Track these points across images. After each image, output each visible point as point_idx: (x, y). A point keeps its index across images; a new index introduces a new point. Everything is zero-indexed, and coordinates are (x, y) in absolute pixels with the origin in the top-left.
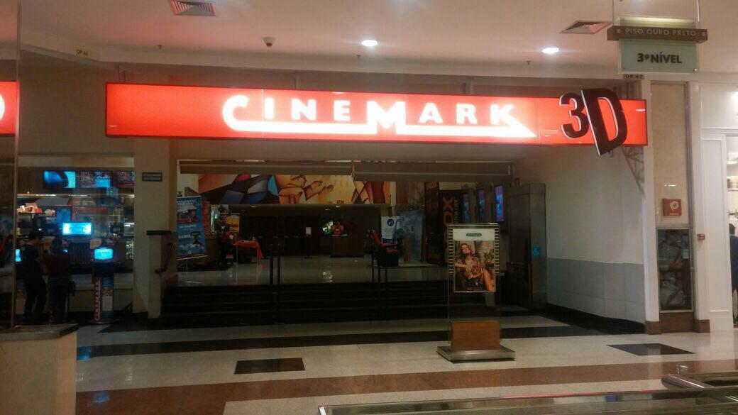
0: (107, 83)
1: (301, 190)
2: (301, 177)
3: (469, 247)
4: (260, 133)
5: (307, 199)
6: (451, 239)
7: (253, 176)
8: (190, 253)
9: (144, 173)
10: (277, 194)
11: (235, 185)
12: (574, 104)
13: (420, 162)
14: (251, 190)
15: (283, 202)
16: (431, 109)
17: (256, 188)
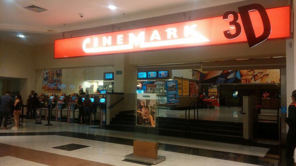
0: (55, 40)
1: (252, 77)
2: (252, 70)
3: (144, 103)
4: (93, 53)
5: (255, 81)
6: (137, 98)
7: (229, 71)
8: (173, 102)
9: (117, 71)
10: (240, 79)
11: (221, 76)
12: (231, 18)
13: (223, 60)
14: (229, 77)
15: (243, 82)
16: (155, 33)
17: (231, 76)
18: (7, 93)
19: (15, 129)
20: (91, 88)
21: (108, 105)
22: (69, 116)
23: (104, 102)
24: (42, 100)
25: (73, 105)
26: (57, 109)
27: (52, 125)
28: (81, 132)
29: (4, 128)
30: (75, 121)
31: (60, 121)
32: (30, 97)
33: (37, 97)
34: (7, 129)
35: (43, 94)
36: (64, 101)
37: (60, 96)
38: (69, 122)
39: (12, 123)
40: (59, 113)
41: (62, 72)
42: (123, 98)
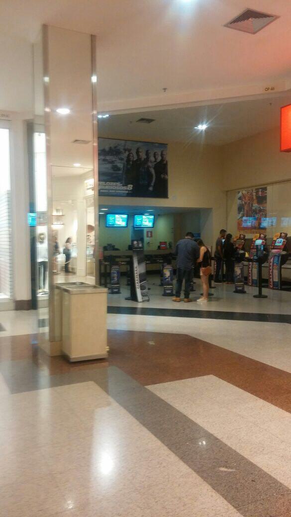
19: (202, 304)
22: (271, 277)
25: (279, 256)
26: (271, 264)
27: (266, 297)
31: (278, 289)
32: (219, 243)
34: (190, 301)
35: (242, 236)
37: (275, 239)
40: (276, 272)
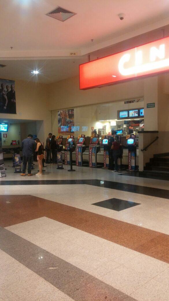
0: (80, 65)
9: (147, 104)
18: (28, 136)
19: (39, 176)
20: (103, 129)
21: (141, 146)
23: (133, 143)
24: (60, 143)
25: (95, 148)
26: (77, 152)
27: (74, 171)
28: (114, 181)
29: (29, 174)
30: (98, 166)
32: (48, 141)
33: (55, 140)
34: (31, 175)
35: (61, 137)
36: (84, 143)
38: (92, 167)
39: (34, 168)
40: (80, 157)
41: (74, 112)
42: (157, 138)
